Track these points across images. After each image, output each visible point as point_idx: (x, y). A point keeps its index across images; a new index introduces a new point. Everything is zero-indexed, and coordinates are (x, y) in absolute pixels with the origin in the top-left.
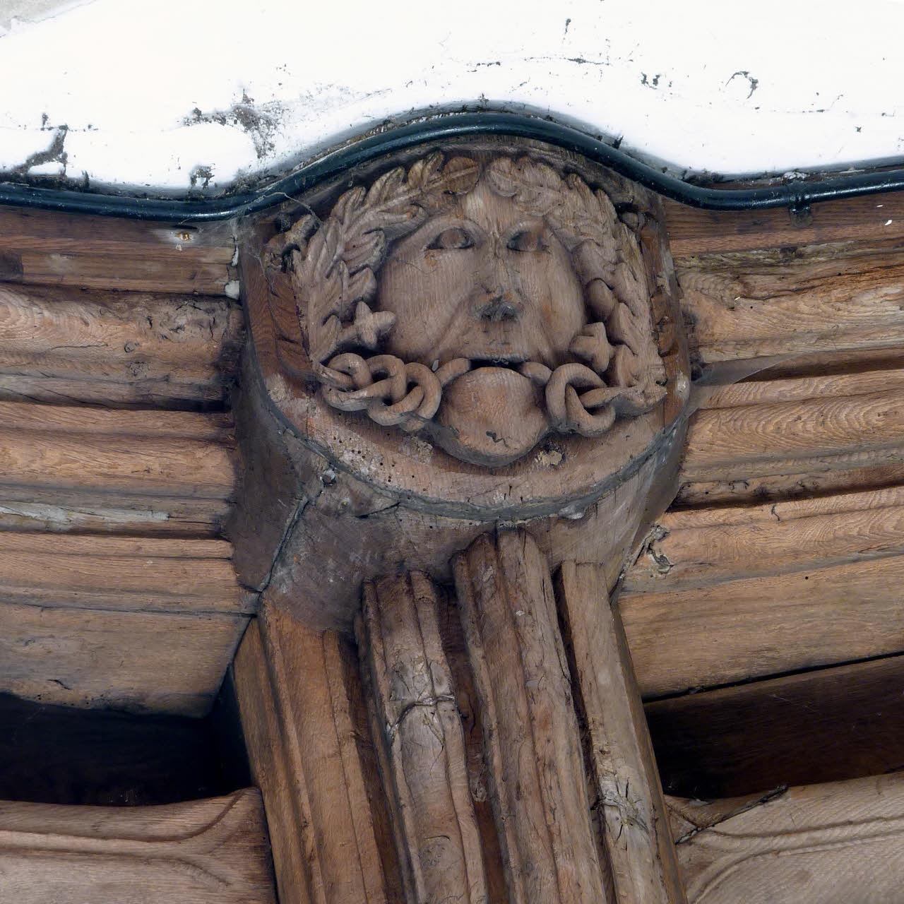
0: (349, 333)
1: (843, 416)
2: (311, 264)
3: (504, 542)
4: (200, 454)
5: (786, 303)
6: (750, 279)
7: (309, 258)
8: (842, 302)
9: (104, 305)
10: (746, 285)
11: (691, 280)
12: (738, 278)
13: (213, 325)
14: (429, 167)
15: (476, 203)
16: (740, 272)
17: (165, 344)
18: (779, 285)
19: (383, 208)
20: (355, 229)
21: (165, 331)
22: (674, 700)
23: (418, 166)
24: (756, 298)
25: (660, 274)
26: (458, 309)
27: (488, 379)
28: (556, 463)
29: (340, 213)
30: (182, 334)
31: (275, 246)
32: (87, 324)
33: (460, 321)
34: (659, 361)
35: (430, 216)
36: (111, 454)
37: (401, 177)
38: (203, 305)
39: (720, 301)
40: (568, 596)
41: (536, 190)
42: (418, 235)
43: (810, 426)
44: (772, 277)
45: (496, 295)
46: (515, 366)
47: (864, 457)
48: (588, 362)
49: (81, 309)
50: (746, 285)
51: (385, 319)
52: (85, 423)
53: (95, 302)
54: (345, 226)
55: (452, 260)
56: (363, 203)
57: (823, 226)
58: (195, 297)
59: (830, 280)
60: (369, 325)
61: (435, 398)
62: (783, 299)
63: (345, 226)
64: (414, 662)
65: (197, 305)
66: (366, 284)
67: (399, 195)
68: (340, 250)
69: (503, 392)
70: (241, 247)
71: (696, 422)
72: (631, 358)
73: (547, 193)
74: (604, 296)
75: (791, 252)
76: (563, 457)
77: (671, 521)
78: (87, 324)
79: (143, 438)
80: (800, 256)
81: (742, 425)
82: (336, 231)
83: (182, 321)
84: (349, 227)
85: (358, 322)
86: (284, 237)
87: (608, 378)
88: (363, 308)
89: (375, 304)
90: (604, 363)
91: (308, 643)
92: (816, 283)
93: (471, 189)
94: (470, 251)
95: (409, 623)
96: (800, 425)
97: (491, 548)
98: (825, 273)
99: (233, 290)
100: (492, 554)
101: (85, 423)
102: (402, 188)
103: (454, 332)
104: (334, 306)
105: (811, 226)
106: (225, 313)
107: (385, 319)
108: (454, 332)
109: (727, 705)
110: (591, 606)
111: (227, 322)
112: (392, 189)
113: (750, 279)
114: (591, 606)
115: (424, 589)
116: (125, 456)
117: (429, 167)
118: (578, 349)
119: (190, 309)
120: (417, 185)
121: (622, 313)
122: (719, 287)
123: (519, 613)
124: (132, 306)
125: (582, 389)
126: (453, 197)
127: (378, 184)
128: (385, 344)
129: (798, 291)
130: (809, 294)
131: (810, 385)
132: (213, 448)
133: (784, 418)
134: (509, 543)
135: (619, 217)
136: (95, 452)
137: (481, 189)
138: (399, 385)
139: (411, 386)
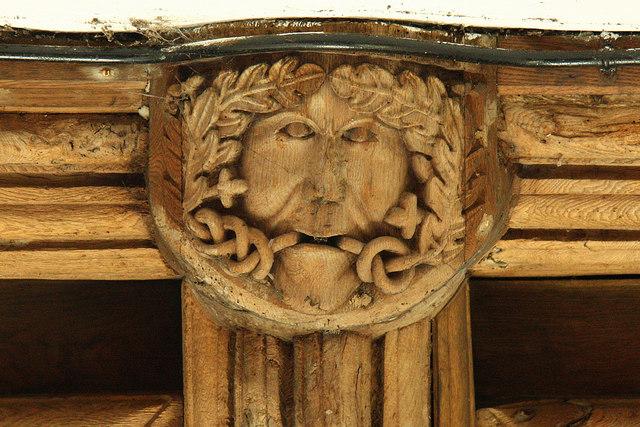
0: (212, 193)
1: (632, 213)
2: (198, 118)
3: (327, 346)
4: (119, 218)
5: (587, 142)
6: (561, 119)
7: (195, 114)
8: (632, 145)
9: (35, 133)
10: (557, 124)
11: (516, 114)
12: (552, 116)
13: (122, 147)
14: (286, 67)
15: (319, 103)
16: (553, 111)
17: (84, 160)
18: (583, 127)
19: (248, 93)
20: (226, 104)
21: (84, 151)
22: (538, 282)
23: (277, 66)
24: (564, 137)
25: (481, 128)
26: (294, 190)
27: (311, 255)
28: (366, 304)
29: (219, 84)
30: (97, 153)
31: (173, 91)
32: (19, 149)
33: (295, 201)
34: (462, 220)
35: (283, 109)
36: (47, 223)
37: (264, 71)
38: (118, 129)
39: (534, 136)
40: (387, 362)
41: (370, 90)
42: (274, 119)
43: (606, 217)
44: (579, 119)
45: (320, 195)
46: (333, 243)
47: (581, 404)
48: (396, 233)
49: (15, 137)
50: (557, 124)
51: (240, 188)
52: (27, 199)
53: (27, 130)
54: (220, 99)
55: (296, 146)
56: (234, 86)
57: (624, 84)
58: (114, 119)
59: (627, 126)
60: (228, 190)
61: (267, 264)
62: (586, 139)
63: (220, 99)
64: (258, 412)
65: (113, 129)
66: (231, 153)
67: (261, 86)
68: (214, 119)
69: (322, 265)
70: (151, 80)
71: (516, 205)
72: (434, 222)
73: (379, 88)
74: (422, 168)
75: (598, 99)
76: (373, 300)
77: (504, 244)
78: (19, 149)
79: (74, 208)
80: (605, 102)
81: (552, 211)
82: (213, 103)
83: (98, 143)
84: (223, 101)
85: (219, 187)
86: (180, 87)
87: (413, 245)
88: (225, 175)
89: (238, 169)
90: (409, 234)
91: (209, 334)
92: (613, 128)
93: (315, 91)
94: (311, 139)
95: (260, 378)
96: (598, 215)
97: (318, 346)
98: (623, 120)
99: (144, 112)
100: (318, 353)
101: (27, 199)
102: (264, 81)
103: (289, 209)
104: (205, 168)
105: (615, 83)
106: (135, 135)
107: (240, 188)
108: (289, 209)
109: (576, 293)
110: (406, 365)
111: (133, 145)
112: (257, 79)
113: (561, 119)
114: (406, 365)
115: (273, 351)
116: (58, 223)
117: (286, 67)
118: (391, 221)
119: (106, 132)
120: (274, 81)
121: (434, 186)
122: (536, 124)
123: (328, 412)
124: (58, 132)
125: (386, 256)
126: (301, 96)
127: (247, 72)
128: (239, 208)
129: (598, 134)
130: (607, 137)
131: (609, 186)
132: (130, 213)
133: (586, 208)
134: (330, 348)
135: (448, 89)
136: (34, 222)
137: (325, 91)
138: (242, 250)
139: (252, 249)
